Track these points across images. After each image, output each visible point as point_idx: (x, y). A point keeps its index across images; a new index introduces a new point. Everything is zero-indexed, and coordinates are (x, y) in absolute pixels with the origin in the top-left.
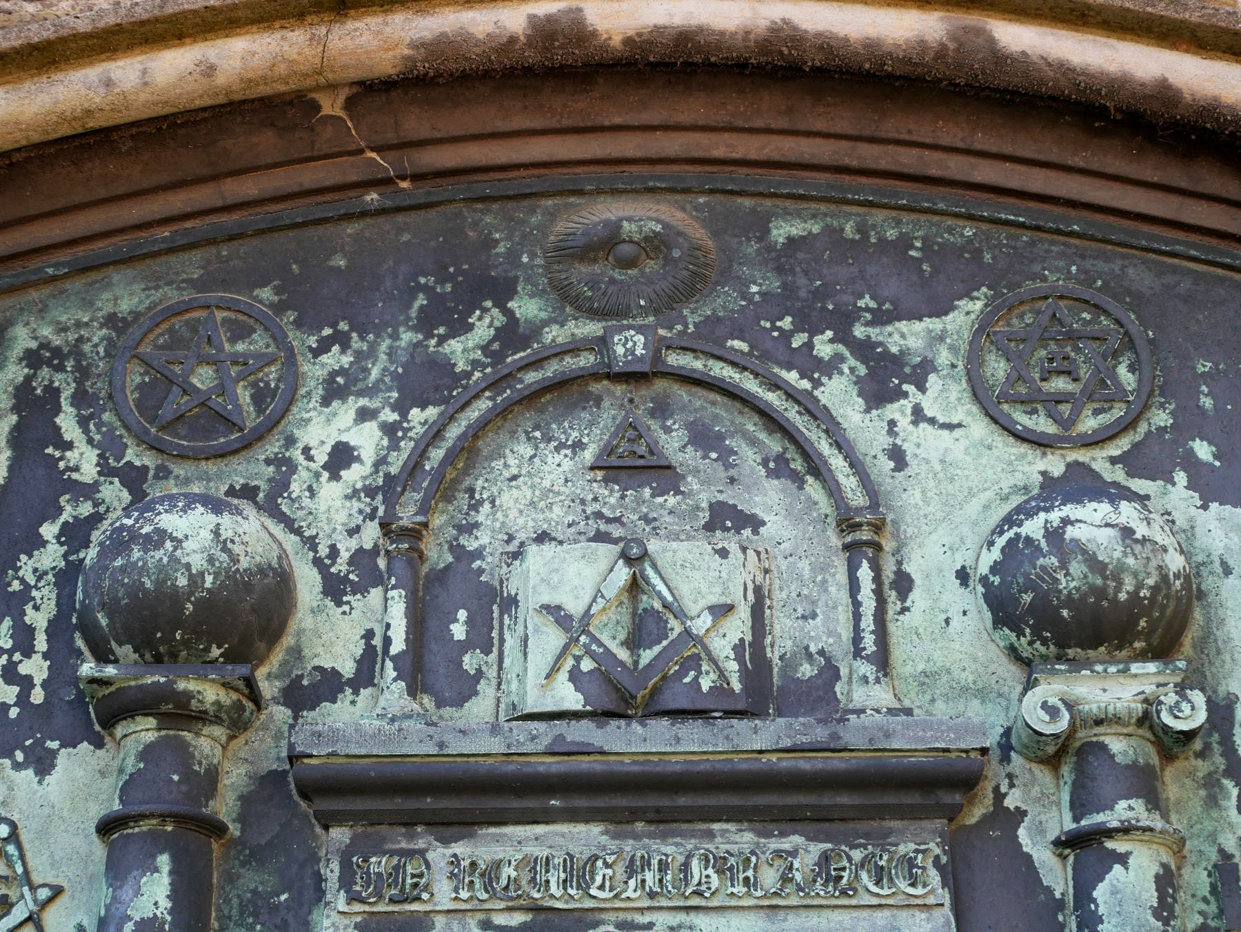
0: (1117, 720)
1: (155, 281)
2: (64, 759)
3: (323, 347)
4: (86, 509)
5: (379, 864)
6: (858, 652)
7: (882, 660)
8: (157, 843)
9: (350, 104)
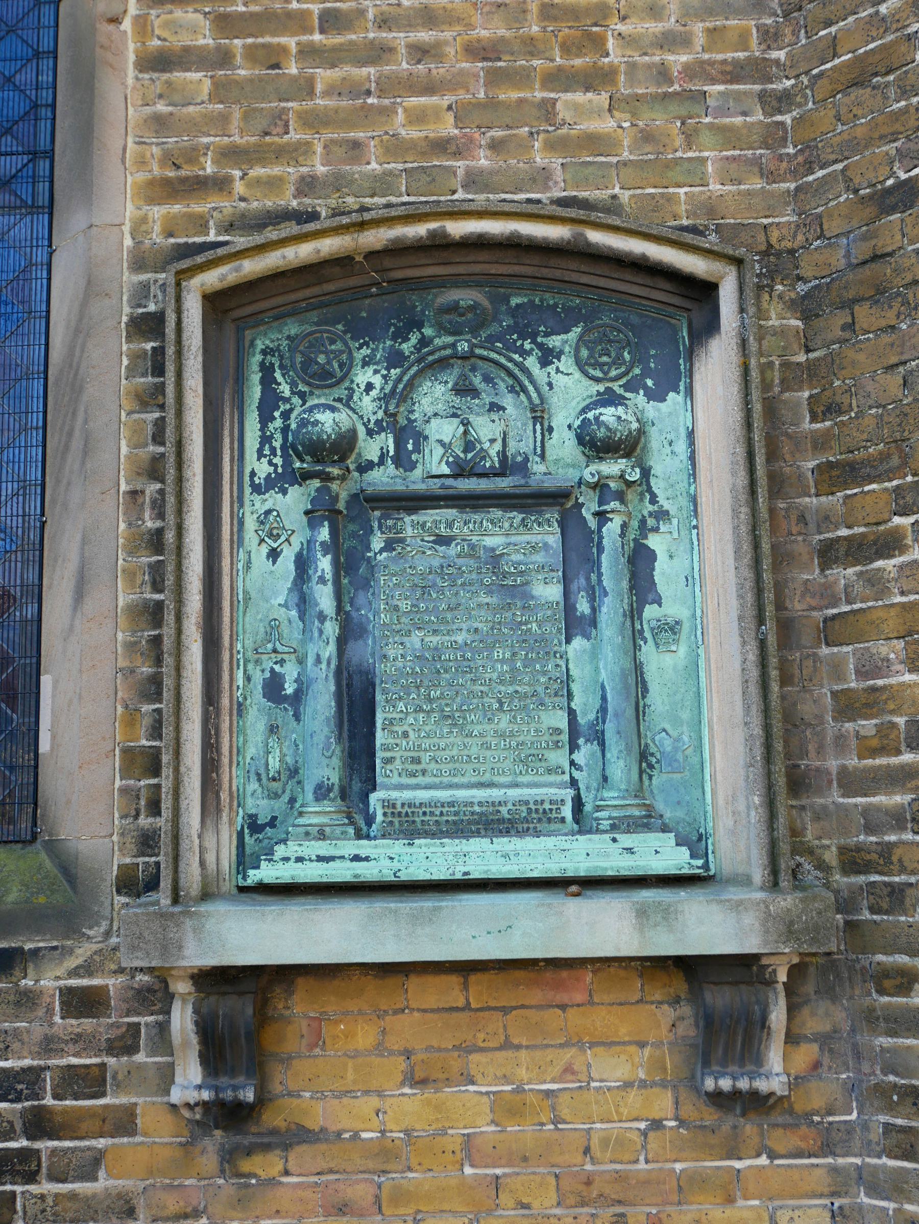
0: (613, 477)
1: (302, 323)
2: (290, 490)
3: (360, 347)
4: (288, 406)
5: (390, 523)
6: (535, 453)
7: (543, 456)
8: (324, 518)
9: (365, 257)
